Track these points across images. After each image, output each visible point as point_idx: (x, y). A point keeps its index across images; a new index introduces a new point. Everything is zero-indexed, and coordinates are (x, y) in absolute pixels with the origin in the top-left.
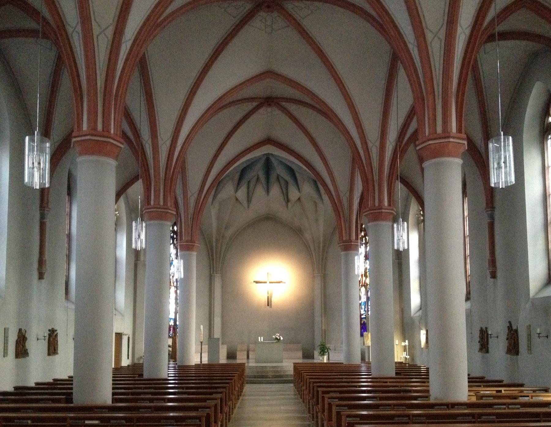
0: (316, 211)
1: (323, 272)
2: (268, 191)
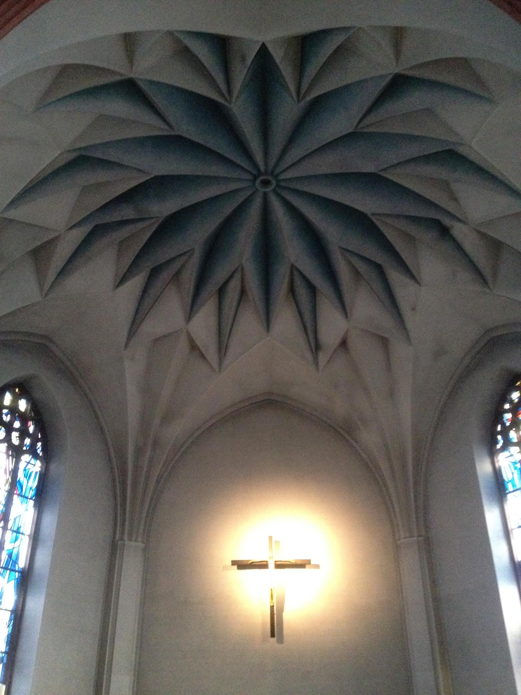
0: (388, 366)
1: (423, 533)
2: (268, 319)
